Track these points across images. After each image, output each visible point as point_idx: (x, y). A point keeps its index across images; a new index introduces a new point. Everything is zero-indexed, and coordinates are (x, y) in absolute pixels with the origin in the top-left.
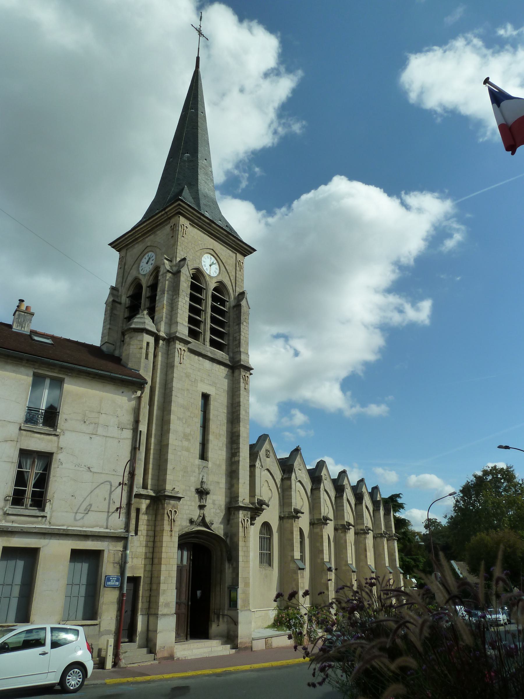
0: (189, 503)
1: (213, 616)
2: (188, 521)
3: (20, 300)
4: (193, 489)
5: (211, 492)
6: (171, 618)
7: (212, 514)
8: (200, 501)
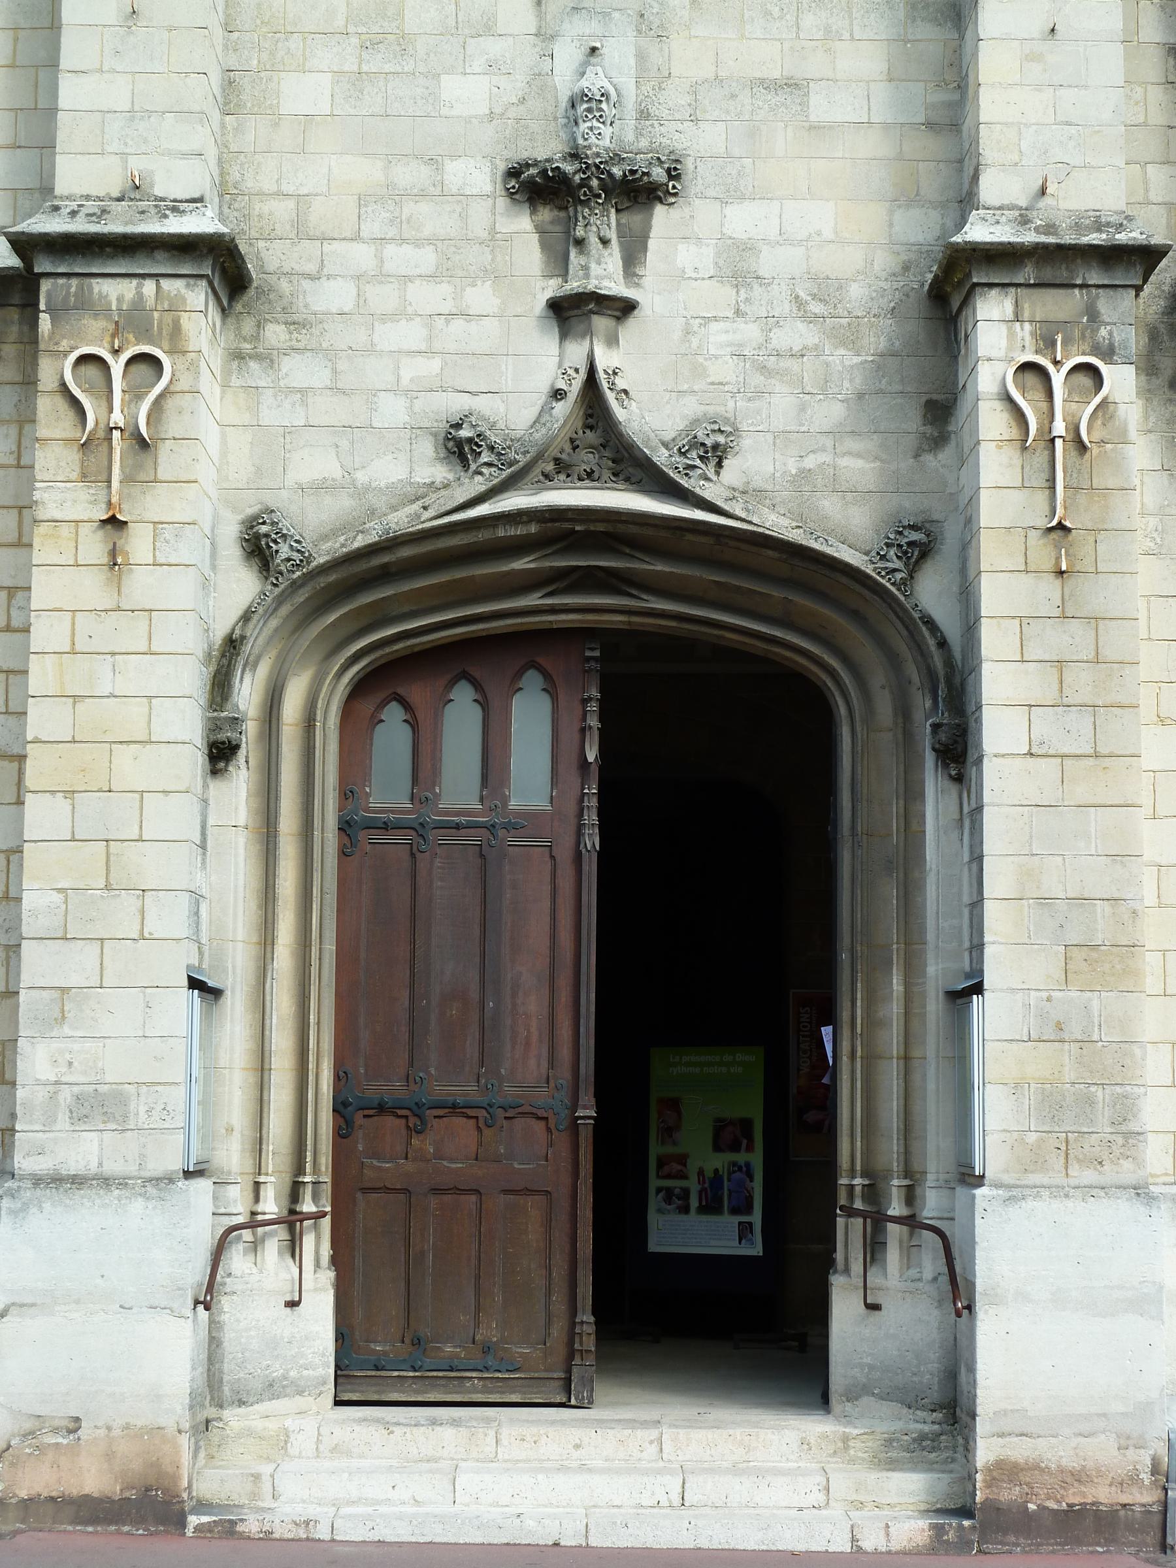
0: (431, 297)
1: (849, 1234)
2: (427, 448)
3: (545, 189)
4: (479, 177)
5: (700, 177)
6: (138, 1205)
7: (725, 370)
8: (559, 264)
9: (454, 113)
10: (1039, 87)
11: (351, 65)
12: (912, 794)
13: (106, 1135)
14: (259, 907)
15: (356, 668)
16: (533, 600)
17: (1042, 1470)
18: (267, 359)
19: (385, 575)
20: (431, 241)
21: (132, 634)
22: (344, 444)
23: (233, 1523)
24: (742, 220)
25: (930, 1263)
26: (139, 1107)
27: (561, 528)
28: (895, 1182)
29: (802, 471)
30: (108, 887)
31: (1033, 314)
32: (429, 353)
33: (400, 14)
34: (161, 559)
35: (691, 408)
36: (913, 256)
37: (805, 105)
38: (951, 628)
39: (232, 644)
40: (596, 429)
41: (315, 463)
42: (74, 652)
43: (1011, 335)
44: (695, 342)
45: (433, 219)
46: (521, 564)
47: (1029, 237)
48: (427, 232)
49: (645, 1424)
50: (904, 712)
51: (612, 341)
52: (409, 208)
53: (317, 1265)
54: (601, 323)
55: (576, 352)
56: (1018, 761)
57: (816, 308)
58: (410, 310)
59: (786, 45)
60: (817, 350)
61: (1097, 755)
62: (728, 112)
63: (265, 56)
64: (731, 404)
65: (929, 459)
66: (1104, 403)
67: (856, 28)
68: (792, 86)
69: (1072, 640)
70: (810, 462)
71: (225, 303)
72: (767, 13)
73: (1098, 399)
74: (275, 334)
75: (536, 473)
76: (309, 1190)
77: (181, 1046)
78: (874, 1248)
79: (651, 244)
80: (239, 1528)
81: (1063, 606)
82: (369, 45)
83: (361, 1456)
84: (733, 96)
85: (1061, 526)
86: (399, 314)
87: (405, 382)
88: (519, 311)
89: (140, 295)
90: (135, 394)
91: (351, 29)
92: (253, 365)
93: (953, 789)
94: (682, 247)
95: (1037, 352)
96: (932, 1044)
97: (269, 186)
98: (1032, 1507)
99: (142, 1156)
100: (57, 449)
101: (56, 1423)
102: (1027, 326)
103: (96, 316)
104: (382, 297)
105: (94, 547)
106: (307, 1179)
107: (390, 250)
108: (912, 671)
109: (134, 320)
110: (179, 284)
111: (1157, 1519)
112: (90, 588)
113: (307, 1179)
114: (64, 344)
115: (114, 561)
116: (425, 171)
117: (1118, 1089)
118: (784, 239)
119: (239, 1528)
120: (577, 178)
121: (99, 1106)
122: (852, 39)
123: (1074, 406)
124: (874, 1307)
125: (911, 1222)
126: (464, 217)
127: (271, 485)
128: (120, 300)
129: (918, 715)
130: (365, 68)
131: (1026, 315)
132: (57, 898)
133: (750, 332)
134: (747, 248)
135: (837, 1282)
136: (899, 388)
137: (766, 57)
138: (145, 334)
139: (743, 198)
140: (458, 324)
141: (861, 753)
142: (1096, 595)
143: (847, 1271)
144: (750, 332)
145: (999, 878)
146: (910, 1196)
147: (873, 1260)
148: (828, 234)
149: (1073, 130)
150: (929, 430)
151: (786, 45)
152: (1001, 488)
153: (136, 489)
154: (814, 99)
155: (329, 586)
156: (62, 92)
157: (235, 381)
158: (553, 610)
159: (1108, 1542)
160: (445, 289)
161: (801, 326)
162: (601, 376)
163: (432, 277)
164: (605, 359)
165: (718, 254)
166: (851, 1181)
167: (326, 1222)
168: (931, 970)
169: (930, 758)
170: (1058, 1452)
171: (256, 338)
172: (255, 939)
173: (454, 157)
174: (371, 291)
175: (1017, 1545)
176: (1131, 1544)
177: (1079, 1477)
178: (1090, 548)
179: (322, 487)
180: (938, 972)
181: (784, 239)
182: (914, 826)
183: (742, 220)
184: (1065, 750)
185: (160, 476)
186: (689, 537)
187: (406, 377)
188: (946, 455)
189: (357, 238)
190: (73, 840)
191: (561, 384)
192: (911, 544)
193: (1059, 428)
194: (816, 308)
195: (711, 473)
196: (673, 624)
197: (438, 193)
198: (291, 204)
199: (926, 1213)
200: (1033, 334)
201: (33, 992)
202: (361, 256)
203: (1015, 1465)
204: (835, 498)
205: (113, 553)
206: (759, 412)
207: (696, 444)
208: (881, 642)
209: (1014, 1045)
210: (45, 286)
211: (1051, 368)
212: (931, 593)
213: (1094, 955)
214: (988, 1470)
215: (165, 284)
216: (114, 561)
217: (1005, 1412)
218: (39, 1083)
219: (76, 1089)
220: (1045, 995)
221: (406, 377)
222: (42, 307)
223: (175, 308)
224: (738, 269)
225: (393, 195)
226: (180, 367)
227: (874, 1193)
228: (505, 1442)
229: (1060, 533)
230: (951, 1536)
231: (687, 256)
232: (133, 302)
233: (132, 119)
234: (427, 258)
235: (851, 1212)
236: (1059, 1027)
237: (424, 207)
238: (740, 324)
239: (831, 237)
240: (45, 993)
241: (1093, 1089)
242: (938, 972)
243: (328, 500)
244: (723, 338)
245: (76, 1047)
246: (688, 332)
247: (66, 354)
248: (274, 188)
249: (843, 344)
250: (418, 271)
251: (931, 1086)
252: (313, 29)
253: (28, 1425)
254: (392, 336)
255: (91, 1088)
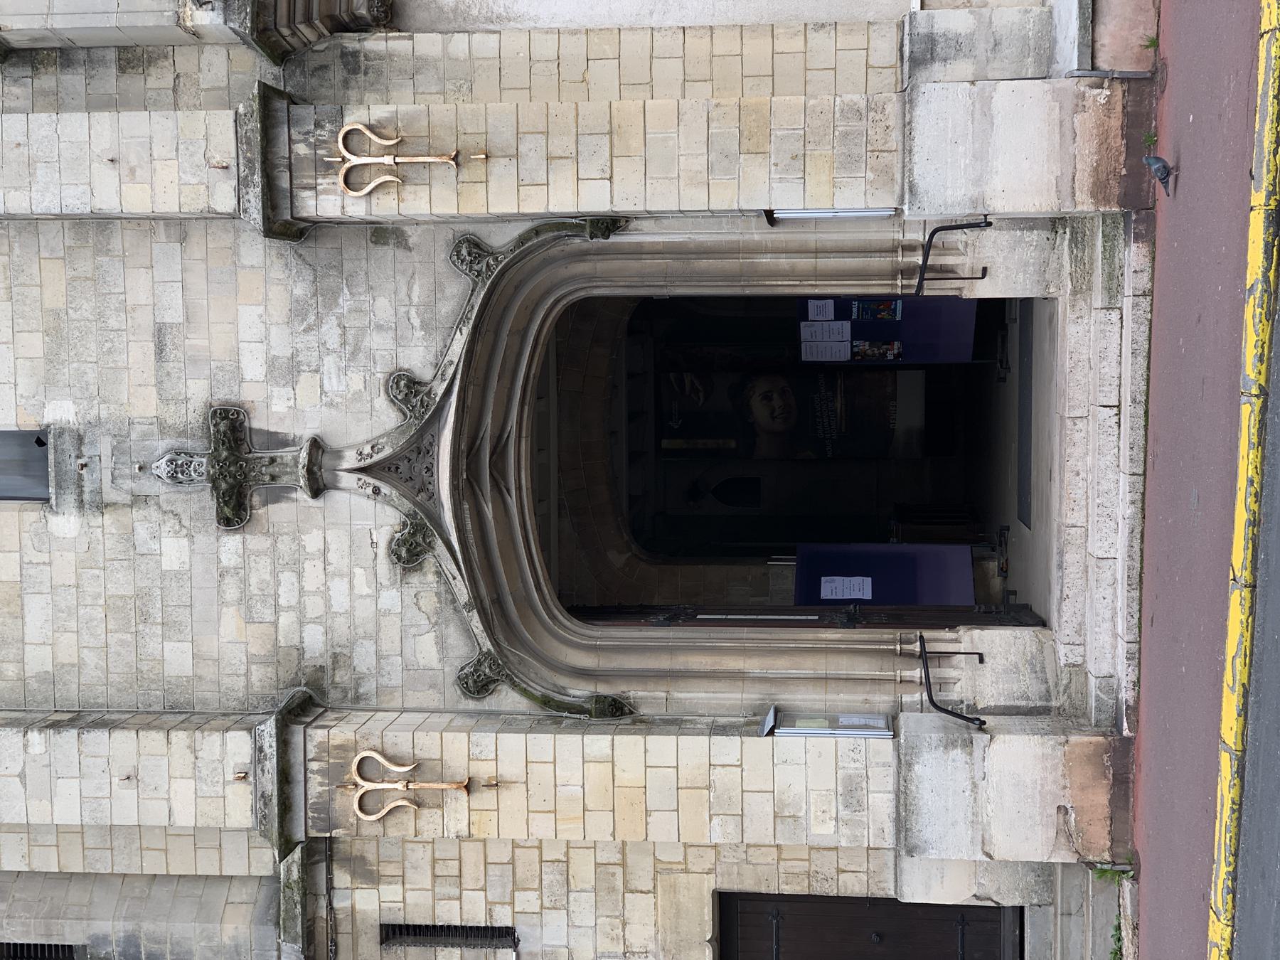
0: (313, 575)
1: (934, 289)
2: (415, 579)
4: (231, 544)
5: (223, 395)
9: (187, 560)
10: (153, 171)
11: (158, 630)
12: (638, 251)
13: (871, 788)
14: (719, 681)
15: (561, 617)
16: (512, 502)
17: (1098, 165)
18: (358, 681)
19: (498, 601)
20: (275, 575)
21: (542, 773)
22: (413, 631)
23: (1128, 707)
24: (254, 368)
25: (957, 237)
26: (852, 767)
27: (466, 485)
28: (900, 259)
29: (422, 328)
30: (709, 788)
31: (310, 177)
32: (351, 576)
33: (122, 597)
34: (493, 756)
35: (381, 402)
36: (273, 253)
37: (171, 325)
38: (528, 225)
39: (546, 702)
40: (398, 469)
41: (426, 650)
42: (555, 812)
43: (326, 192)
44: (338, 400)
45: (260, 572)
46: (489, 511)
47: (257, 178)
48: (268, 577)
49: (1063, 425)
50: (582, 255)
51: (338, 454)
52: (254, 589)
53: (957, 641)
54: (327, 461)
55: (348, 480)
56: (615, 187)
57: (311, 318)
58: (322, 588)
59: (131, 338)
60: (340, 317)
61: (610, 133)
62: (179, 378)
63: (153, 686)
64: (379, 375)
65: (411, 241)
66: (370, 127)
67: (116, 290)
68: (160, 333)
69: (532, 147)
70: (416, 322)
71: (321, 710)
72: (110, 351)
73: (368, 133)
74: (342, 676)
75: (429, 504)
76: (906, 647)
77: (811, 741)
78: (946, 273)
79: (272, 429)
80: (1131, 703)
81: (510, 157)
82: (145, 618)
83: (1083, 615)
84: (168, 374)
85: (455, 159)
86: (325, 594)
87: (369, 591)
88: (320, 517)
89: (318, 772)
90: (383, 775)
91: (133, 629)
92: (361, 691)
93: (633, 224)
94: (274, 408)
95: (337, 174)
96: (811, 238)
97: (242, 682)
98: (1124, 172)
99: (884, 765)
100: (422, 824)
101: (1061, 821)
102: (319, 181)
103: (332, 800)
104: (314, 607)
105: (485, 799)
106: (898, 648)
107: (282, 601)
108: (555, 251)
109: (335, 776)
110: (310, 747)
111: (1133, 84)
112: (512, 799)
113: (898, 648)
114: (352, 820)
115: (495, 784)
116: (228, 579)
117: (837, 115)
118: (265, 340)
119: (1131, 703)
120: (231, 480)
121: (852, 794)
122: (124, 293)
123: (373, 149)
124: (985, 270)
125: (927, 248)
126: (258, 554)
127: (441, 678)
128: (321, 784)
129: (585, 246)
130: (159, 620)
131: (311, 181)
132: (715, 820)
133: (330, 362)
134: (272, 364)
135: (967, 294)
136: (364, 262)
137: (141, 352)
138: (344, 767)
139: (238, 368)
140: (332, 556)
141: (612, 277)
142: (503, 136)
143: (960, 289)
144: (330, 362)
145: (695, 199)
146: (909, 248)
147: (952, 271)
148: (261, 310)
149: (181, 147)
150: (392, 242)
151: (131, 338)
152: (431, 201)
153: (447, 773)
154: (168, 319)
155: (507, 640)
156: (184, 824)
157: (374, 702)
158: (519, 488)
159: (1149, 119)
160: (307, 565)
161: (324, 328)
162: (362, 464)
163: (300, 575)
164: (350, 460)
165: (278, 384)
166: (899, 286)
167: (927, 634)
168: (756, 237)
169: (614, 239)
170: (1086, 154)
171: (345, 691)
172: (740, 684)
173: (219, 561)
174: (311, 614)
175: (1150, 182)
176: (1150, 103)
177: (1104, 138)
178: (468, 138)
179: (441, 643)
180: (759, 233)
181: (265, 340)
182: (660, 247)
183: (254, 368)
184: (608, 154)
185: (438, 756)
186: (469, 401)
187: (366, 590)
188: (408, 230)
189: (275, 624)
190: (678, 810)
191: (369, 491)
192: (469, 254)
193: (388, 160)
194: (311, 318)
195: (426, 389)
196: (526, 408)
197: (242, 574)
198: (254, 667)
199: (921, 239)
200: (324, 177)
201: (778, 835)
202: (286, 620)
203: (1094, 184)
204: (440, 305)
205: (489, 786)
206: (383, 357)
207: (406, 401)
208: (535, 271)
209: (808, 188)
210: (313, 833)
211: (347, 165)
212: (501, 238)
213: (746, 133)
214: (1097, 203)
215: (310, 756)
216: (495, 784)
217: (1058, 191)
218: (837, 831)
219: (841, 808)
220: (773, 168)
221: (366, 590)
222: (328, 835)
223: (325, 748)
224: (287, 371)
225: (245, 600)
226: (366, 745)
227: (907, 272)
228: (1074, 522)
229: (460, 158)
230: (1142, 228)
231: (279, 406)
232: (322, 776)
233: (200, 778)
234: (287, 577)
235: (920, 287)
236: (795, 157)
237: (253, 580)
238: (324, 369)
239: (262, 308)
240: (778, 828)
241: (837, 133)
242: (759, 233)
243: (451, 641)
244: (334, 380)
245: (813, 808)
246: (331, 405)
247: (358, 819)
248: (243, 678)
249: (336, 300)
250: (296, 584)
251: (835, 237)
252: (134, 654)
253: (1063, 840)
254: (340, 599)
255: (840, 799)
